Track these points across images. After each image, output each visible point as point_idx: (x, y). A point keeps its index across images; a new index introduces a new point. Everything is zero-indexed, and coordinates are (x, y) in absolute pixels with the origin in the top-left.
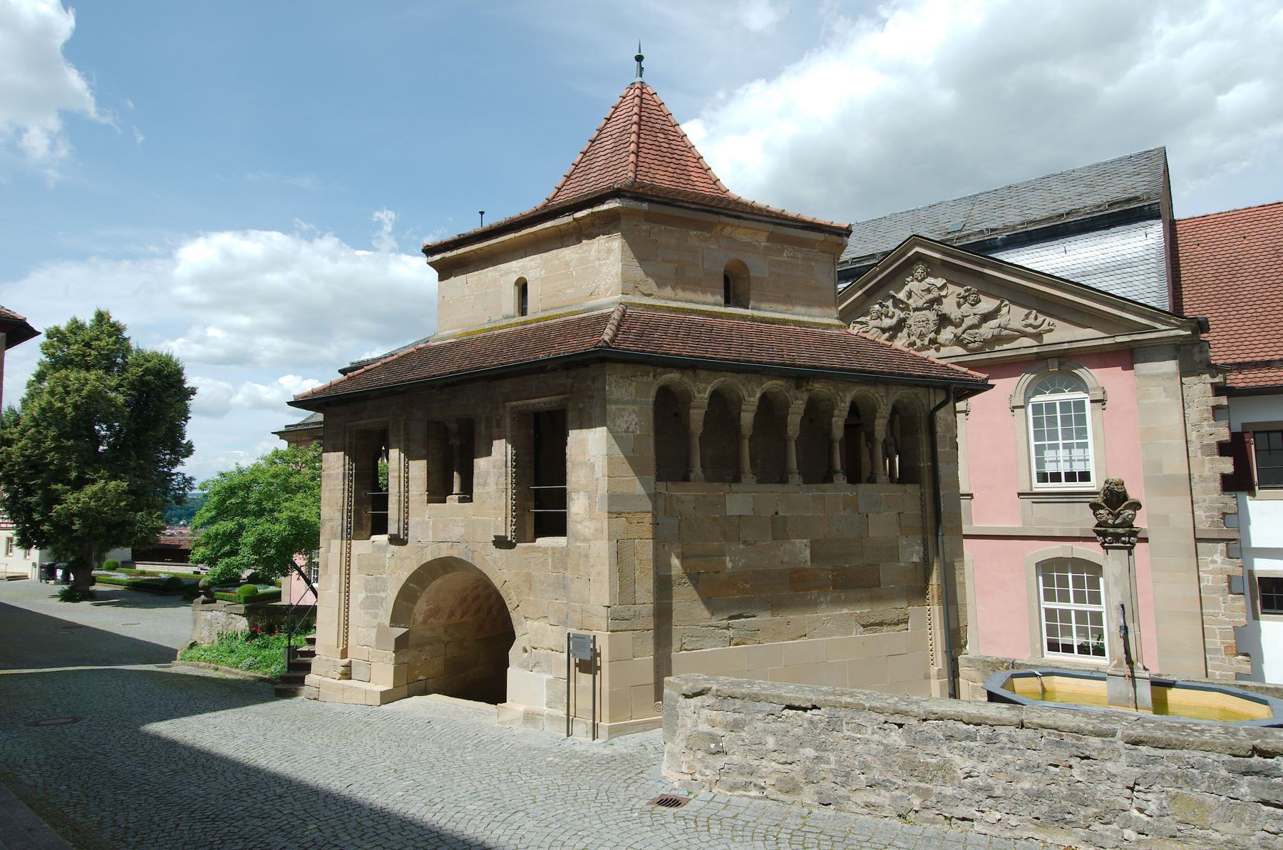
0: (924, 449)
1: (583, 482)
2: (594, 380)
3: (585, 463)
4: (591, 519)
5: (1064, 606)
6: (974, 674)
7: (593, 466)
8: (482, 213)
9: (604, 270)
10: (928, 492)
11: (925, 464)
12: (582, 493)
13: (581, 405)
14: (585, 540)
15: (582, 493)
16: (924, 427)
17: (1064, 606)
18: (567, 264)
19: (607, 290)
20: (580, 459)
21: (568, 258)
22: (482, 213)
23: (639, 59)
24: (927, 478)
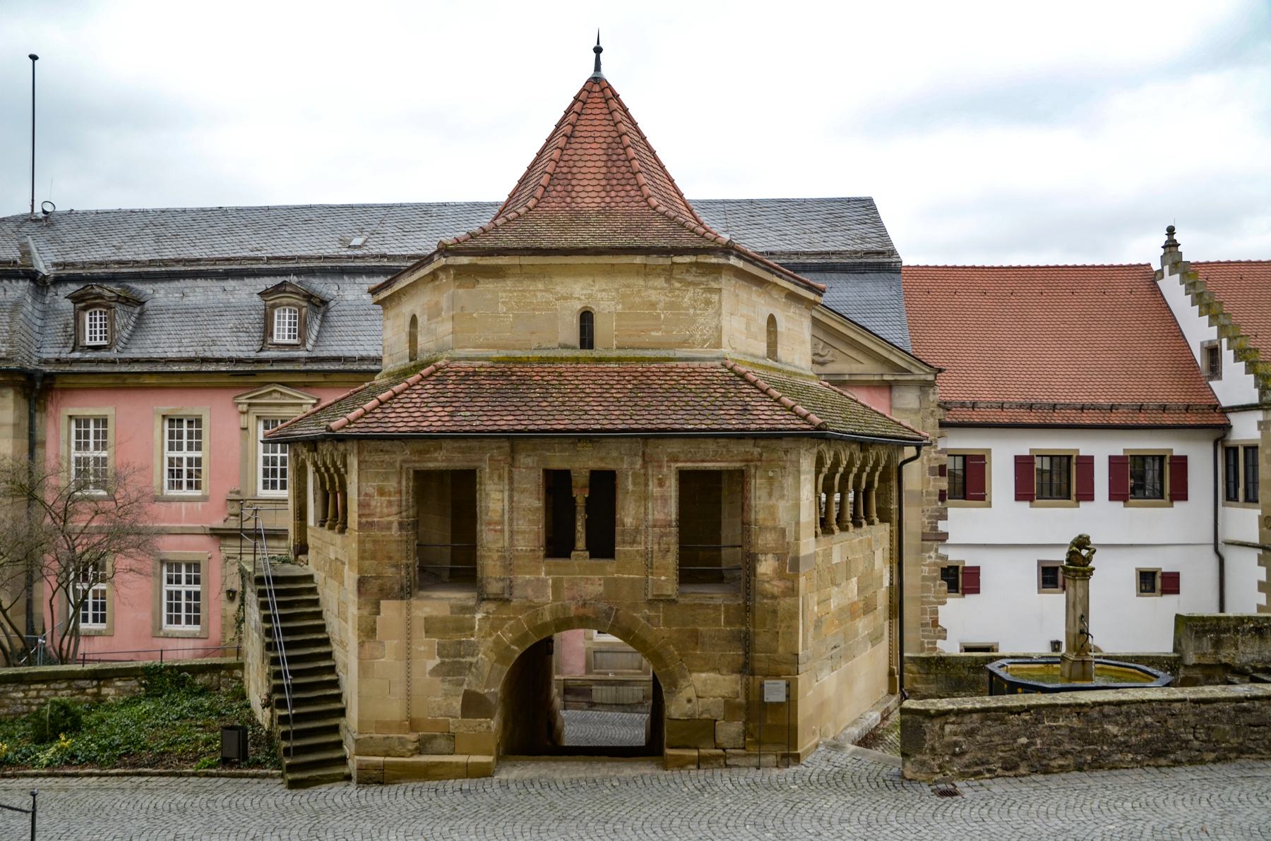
0: (895, 494)
1: (772, 544)
2: (786, 452)
3: (775, 528)
4: (781, 579)
5: (97, 454)
6: (914, 668)
7: (783, 531)
8: (34, 58)
9: (701, 320)
10: (895, 528)
11: (894, 506)
12: (770, 556)
13: (771, 474)
14: (774, 597)
15: (770, 556)
16: (895, 476)
17: (97, 454)
18: (653, 305)
19: (705, 341)
20: (769, 523)
21: (653, 298)
22: (34, 58)
23: (598, 50)
24: (895, 517)
